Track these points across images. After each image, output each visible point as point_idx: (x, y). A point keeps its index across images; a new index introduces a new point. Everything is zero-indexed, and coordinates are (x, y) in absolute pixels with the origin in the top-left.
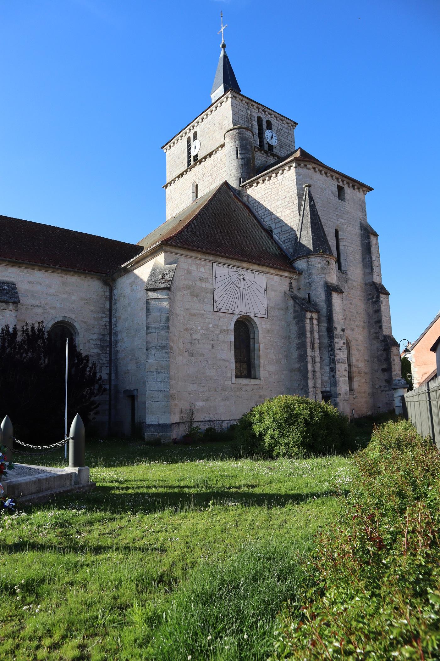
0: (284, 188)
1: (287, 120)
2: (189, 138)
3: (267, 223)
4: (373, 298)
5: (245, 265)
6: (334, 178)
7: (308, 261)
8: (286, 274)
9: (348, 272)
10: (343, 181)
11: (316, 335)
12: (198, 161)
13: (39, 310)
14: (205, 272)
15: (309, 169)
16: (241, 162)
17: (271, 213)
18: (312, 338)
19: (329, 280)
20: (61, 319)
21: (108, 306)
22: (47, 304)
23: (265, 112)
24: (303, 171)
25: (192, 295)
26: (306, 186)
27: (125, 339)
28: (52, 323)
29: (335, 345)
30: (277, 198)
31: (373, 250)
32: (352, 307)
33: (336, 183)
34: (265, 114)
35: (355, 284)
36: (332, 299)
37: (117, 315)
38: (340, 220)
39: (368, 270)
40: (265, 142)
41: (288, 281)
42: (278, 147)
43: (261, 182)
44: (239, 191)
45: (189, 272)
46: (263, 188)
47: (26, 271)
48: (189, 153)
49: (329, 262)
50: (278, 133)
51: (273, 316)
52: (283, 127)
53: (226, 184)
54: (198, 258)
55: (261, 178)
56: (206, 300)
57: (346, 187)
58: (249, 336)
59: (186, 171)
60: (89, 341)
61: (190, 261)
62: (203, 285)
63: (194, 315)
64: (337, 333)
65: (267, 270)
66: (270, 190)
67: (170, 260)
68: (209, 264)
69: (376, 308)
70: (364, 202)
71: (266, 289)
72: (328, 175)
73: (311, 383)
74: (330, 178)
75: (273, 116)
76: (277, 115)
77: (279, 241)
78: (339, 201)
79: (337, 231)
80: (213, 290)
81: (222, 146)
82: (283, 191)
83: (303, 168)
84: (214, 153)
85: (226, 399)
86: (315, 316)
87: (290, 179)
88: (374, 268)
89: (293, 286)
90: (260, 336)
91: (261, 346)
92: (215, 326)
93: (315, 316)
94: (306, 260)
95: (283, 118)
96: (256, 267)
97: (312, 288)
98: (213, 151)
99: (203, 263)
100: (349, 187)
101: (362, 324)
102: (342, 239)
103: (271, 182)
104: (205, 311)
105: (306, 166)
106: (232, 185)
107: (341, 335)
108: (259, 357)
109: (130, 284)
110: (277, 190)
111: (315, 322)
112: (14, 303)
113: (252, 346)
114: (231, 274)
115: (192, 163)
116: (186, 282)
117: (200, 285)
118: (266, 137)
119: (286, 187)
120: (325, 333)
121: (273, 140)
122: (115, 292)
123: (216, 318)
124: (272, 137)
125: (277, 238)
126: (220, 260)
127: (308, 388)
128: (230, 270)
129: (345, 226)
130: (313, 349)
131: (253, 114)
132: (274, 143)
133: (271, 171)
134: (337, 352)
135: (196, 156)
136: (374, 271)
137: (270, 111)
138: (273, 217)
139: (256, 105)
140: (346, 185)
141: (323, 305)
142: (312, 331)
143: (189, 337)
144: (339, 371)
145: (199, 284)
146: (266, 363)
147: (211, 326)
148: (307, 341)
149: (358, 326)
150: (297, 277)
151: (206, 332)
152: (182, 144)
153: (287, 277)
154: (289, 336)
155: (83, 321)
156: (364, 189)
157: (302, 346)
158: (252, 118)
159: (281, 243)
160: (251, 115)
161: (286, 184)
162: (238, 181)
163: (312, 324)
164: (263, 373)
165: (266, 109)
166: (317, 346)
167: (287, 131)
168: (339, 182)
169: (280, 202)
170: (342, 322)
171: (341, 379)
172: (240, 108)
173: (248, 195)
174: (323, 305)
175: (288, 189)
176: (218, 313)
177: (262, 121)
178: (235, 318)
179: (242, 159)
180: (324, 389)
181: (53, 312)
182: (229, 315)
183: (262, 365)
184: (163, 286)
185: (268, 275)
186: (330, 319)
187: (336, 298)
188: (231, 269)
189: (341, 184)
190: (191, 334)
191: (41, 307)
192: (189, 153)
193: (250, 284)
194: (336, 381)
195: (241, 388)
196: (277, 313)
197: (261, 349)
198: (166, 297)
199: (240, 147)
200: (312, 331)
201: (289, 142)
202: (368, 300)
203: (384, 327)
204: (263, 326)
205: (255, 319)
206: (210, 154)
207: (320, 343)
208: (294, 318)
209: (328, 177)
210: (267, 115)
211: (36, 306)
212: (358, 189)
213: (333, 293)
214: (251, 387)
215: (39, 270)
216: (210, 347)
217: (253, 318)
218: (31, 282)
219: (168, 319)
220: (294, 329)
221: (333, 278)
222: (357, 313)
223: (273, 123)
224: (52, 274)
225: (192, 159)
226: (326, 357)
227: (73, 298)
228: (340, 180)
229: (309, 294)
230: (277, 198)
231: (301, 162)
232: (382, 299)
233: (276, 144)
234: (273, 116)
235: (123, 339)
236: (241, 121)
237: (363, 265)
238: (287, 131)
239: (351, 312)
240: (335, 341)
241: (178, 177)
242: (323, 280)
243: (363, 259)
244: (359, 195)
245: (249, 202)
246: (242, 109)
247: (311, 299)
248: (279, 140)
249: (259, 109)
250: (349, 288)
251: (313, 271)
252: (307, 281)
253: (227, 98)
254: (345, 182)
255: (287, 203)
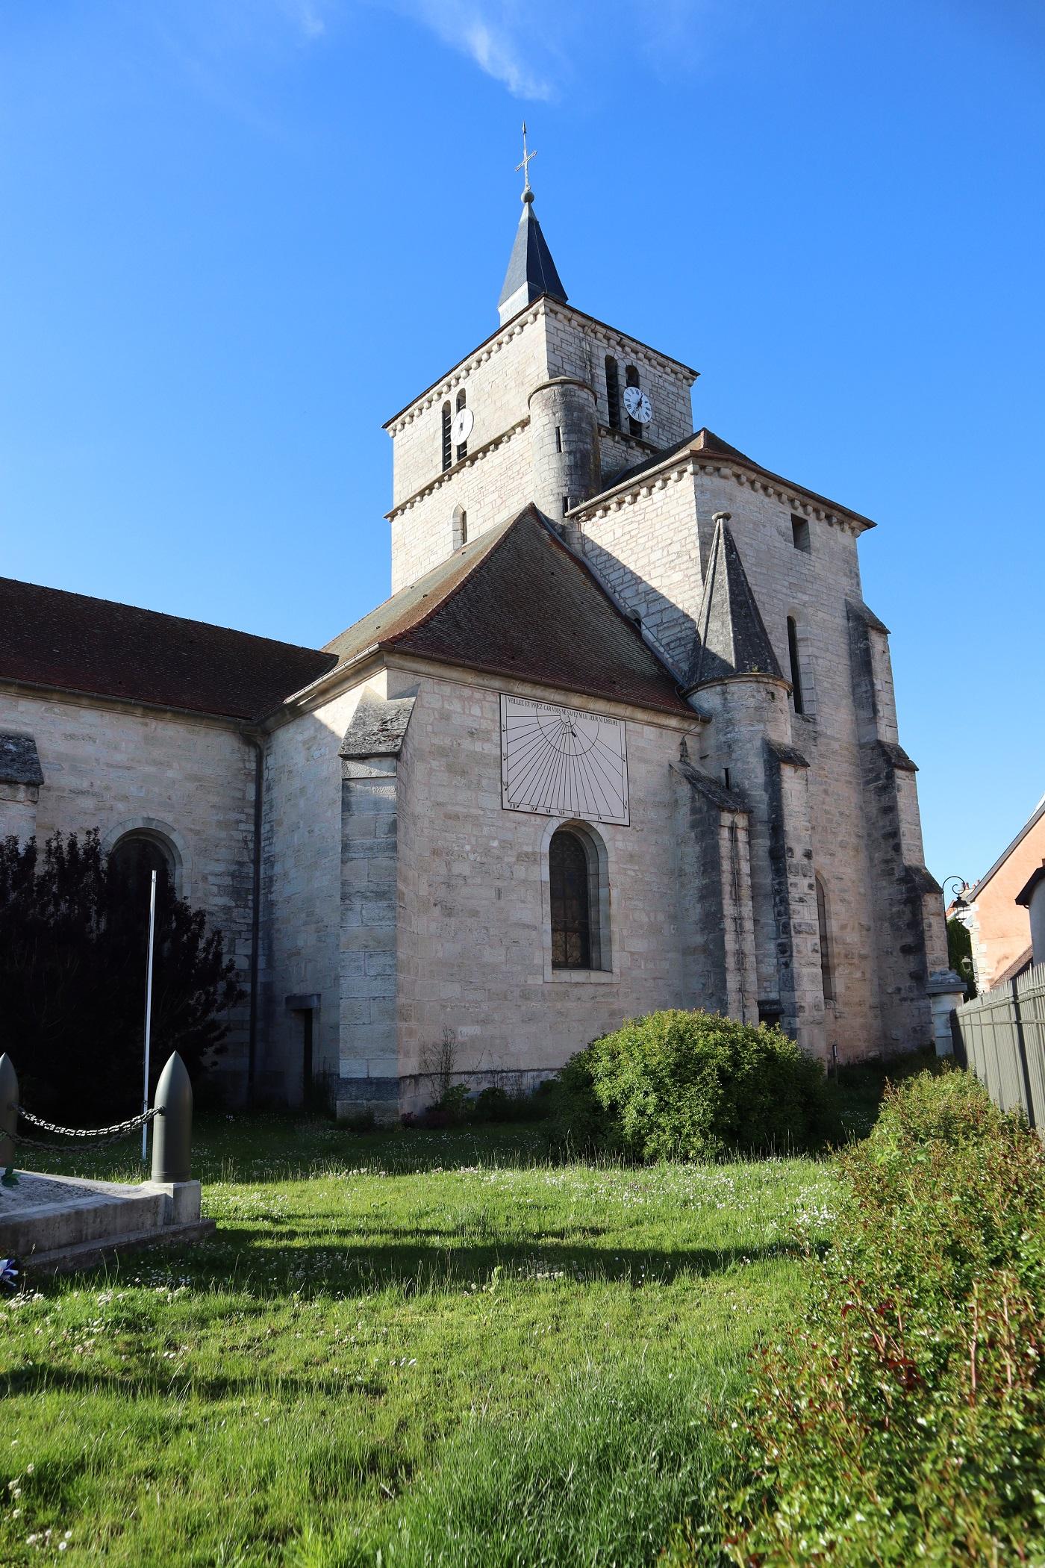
0: (667, 522)
1: (674, 366)
2: (447, 404)
3: (628, 601)
4: (877, 778)
5: (576, 700)
6: (784, 497)
7: (724, 693)
8: (673, 722)
9: (818, 718)
10: (804, 506)
11: (745, 868)
12: (466, 457)
13: (88, 803)
14: (482, 717)
15: (725, 477)
16: (567, 460)
17: (638, 580)
18: (736, 873)
19: (774, 736)
20: (140, 824)
21: (251, 795)
22: (107, 788)
23: (623, 347)
24: (712, 482)
25: (451, 769)
26: (719, 517)
27: (292, 874)
28: (119, 832)
29: (790, 889)
30: (650, 544)
31: (877, 665)
32: (828, 799)
33: (789, 511)
34: (623, 351)
35: (836, 746)
36: (780, 782)
37: (274, 816)
38: (800, 595)
39: (866, 714)
40: (624, 415)
41: (677, 738)
42: (653, 427)
43: (613, 506)
44: (563, 527)
45: (445, 717)
46: (618, 520)
47: (59, 709)
48: (447, 439)
49: (773, 695)
50: (654, 393)
51: (642, 822)
52: (665, 381)
53: (532, 510)
54: (465, 685)
55: (615, 499)
56: (484, 782)
57: (811, 519)
58: (586, 869)
59: (440, 481)
60: (205, 878)
61: (447, 689)
62: (478, 747)
63: (456, 817)
64: (794, 861)
65: (628, 711)
66: (635, 525)
67: (400, 689)
68: (492, 698)
69: (885, 801)
70: (854, 555)
71: (625, 758)
72: (771, 491)
73: (732, 981)
74: (774, 499)
75: (641, 355)
76: (651, 353)
77: (657, 644)
78: (797, 551)
79: (791, 623)
80: (502, 758)
81: (525, 423)
82: (666, 529)
83: (710, 474)
84: (505, 439)
85: (530, 1019)
86: (742, 821)
87: (680, 501)
88: (880, 708)
89: (689, 750)
90: (612, 868)
91: (614, 893)
92: (506, 845)
93: (742, 821)
94: (718, 688)
95: (664, 360)
96: (601, 706)
97: (734, 756)
98: (503, 436)
99: (478, 695)
100: (818, 519)
101: (853, 840)
102: (803, 639)
103: (636, 506)
104: (482, 809)
105: (718, 470)
106: (547, 514)
107: (803, 867)
108: (608, 918)
109: (304, 743)
110: (652, 525)
111: (742, 836)
112: (28, 784)
113: (592, 892)
114: (543, 721)
115: (454, 461)
116: (437, 741)
117: (471, 748)
118: (626, 403)
119: (672, 520)
120: (765, 863)
121: (643, 410)
122: (270, 761)
123: (507, 824)
124: (639, 404)
125: (651, 637)
126: (519, 688)
127: (725, 994)
128: (540, 712)
129: (811, 610)
130: (737, 900)
131: (595, 350)
132: (643, 416)
133: (638, 483)
134: (794, 906)
135: (464, 445)
136: (881, 714)
137: (634, 344)
138: (641, 588)
139: (604, 331)
140: (813, 515)
141: (759, 796)
142: (735, 858)
143: (443, 871)
144: (799, 952)
145: (467, 744)
146: (625, 932)
147: (495, 844)
148: (724, 880)
149: (843, 846)
150: (698, 730)
151: (484, 860)
152: (432, 417)
153: (675, 729)
154: (681, 870)
155: (191, 830)
156: (855, 524)
157: (711, 893)
158: (594, 360)
159: (662, 650)
160: (591, 354)
161: (672, 513)
162: (560, 504)
163: (734, 840)
164: (618, 958)
165: (626, 341)
166: (746, 892)
167: (674, 390)
168: (795, 508)
169: (658, 554)
170: (805, 835)
171: (805, 971)
172: (567, 337)
173: (583, 537)
174: (759, 796)
175: (677, 524)
176: (512, 814)
177: (616, 367)
178: (554, 825)
179: (570, 453)
180: (763, 997)
181: (121, 806)
182: (538, 819)
183: (616, 937)
184: (382, 748)
185: (631, 725)
186: (777, 829)
187: (791, 779)
188: (543, 710)
189: (800, 513)
190: (448, 864)
191: (94, 795)
192: (447, 439)
193: (587, 746)
194: (792, 977)
195: (566, 994)
196: (652, 814)
197: (613, 900)
198: (390, 774)
199: (566, 426)
200: (735, 858)
201: (678, 415)
202: (867, 783)
203: (904, 847)
204: (620, 845)
205: (601, 829)
206: (497, 443)
207: (753, 886)
208: (693, 826)
209: (769, 496)
210: (627, 354)
211: (82, 793)
212: (841, 523)
213: (783, 766)
214: (590, 990)
215: (91, 707)
216: (493, 894)
217: (594, 825)
218: (72, 737)
219: (393, 827)
220: (692, 851)
221: (784, 732)
222: (841, 814)
223: (641, 371)
224: (122, 717)
225: (454, 452)
226: (769, 919)
227: (170, 774)
228: (797, 503)
229: (727, 770)
230: (650, 544)
231: (706, 462)
232: (898, 781)
233: (648, 419)
234: (641, 355)
235: (286, 874)
236: (567, 367)
237: (854, 701)
238: (674, 390)
239: (827, 812)
240: (790, 881)
241: (422, 494)
242: (760, 735)
243: (855, 687)
244: (841, 537)
245: (585, 554)
246: (571, 339)
247: (732, 781)
248: (656, 410)
249: (609, 339)
250: (822, 756)
251: (737, 715)
252: (723, 739)
253: (535, 315)
254: (810, 509)
255: (674, 556)
